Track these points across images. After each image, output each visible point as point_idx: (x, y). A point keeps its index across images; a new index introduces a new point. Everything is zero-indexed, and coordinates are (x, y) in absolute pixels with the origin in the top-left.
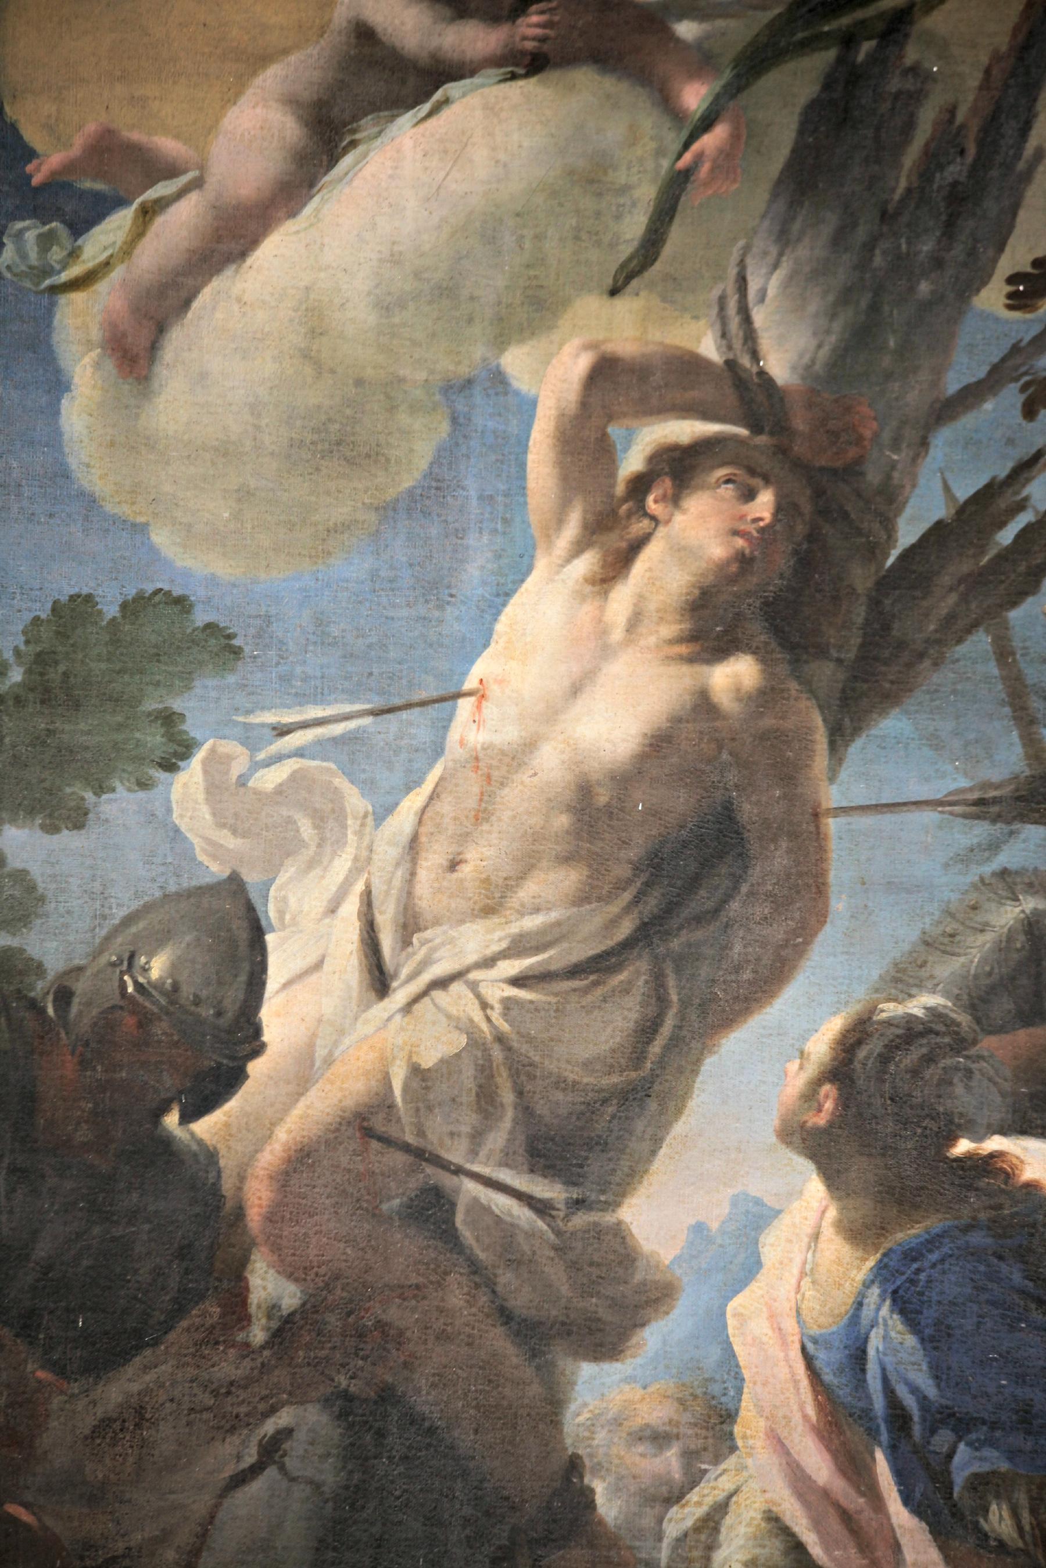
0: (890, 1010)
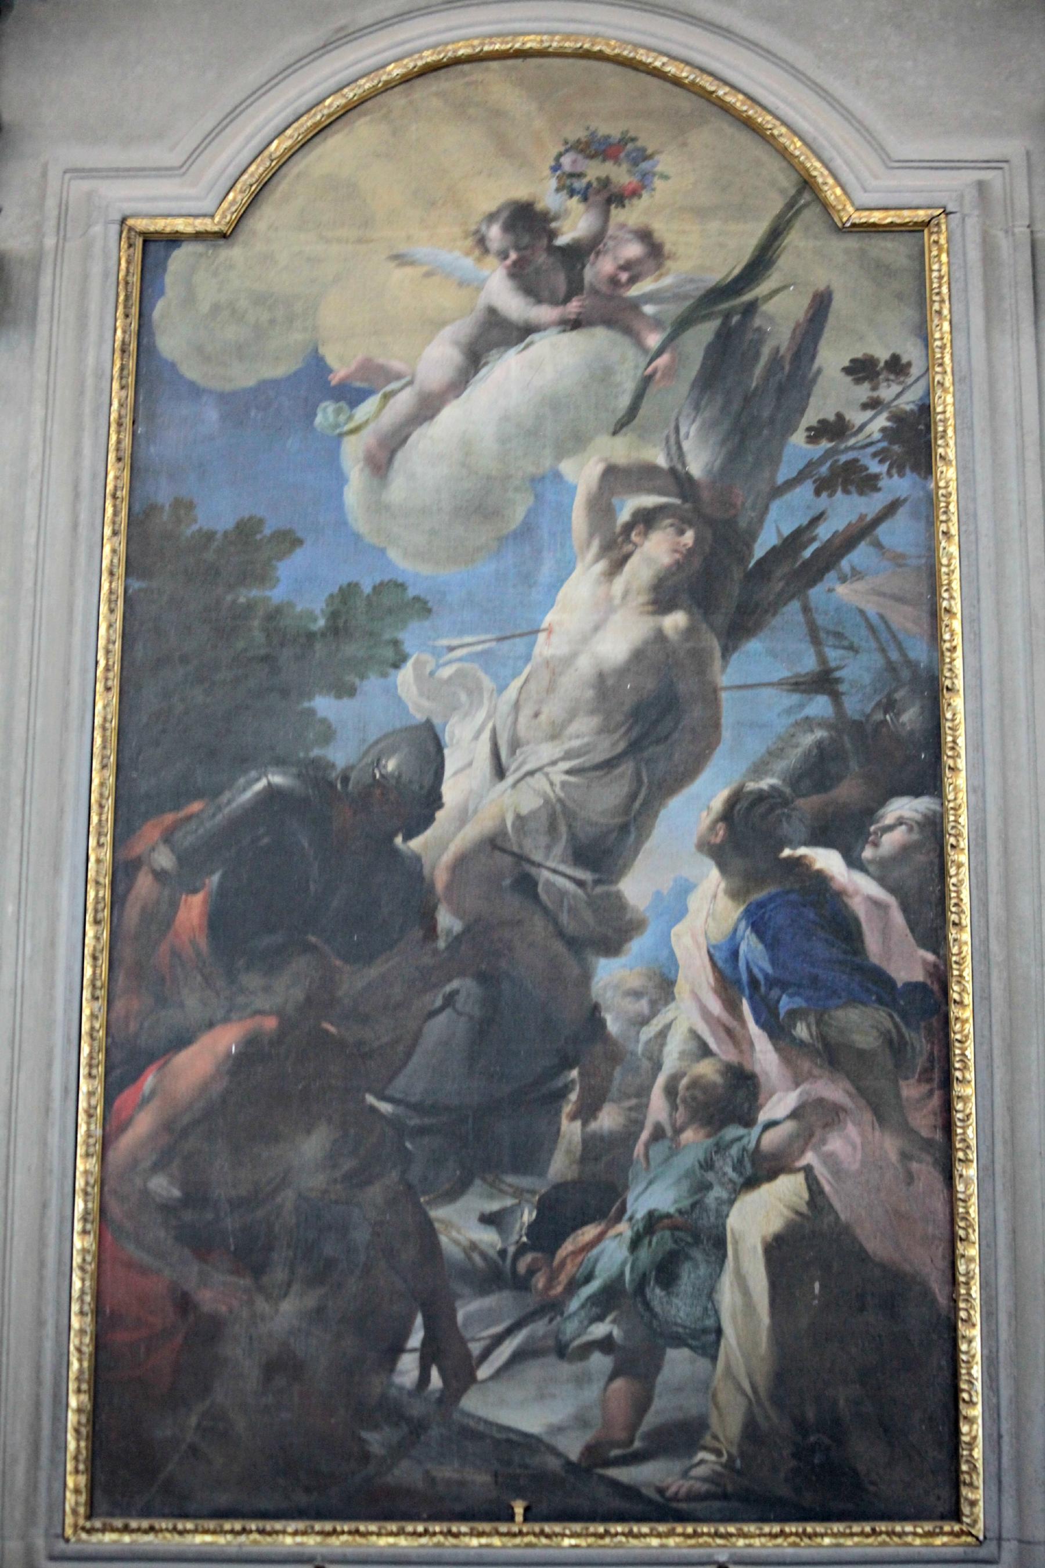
0: (751, 786)
